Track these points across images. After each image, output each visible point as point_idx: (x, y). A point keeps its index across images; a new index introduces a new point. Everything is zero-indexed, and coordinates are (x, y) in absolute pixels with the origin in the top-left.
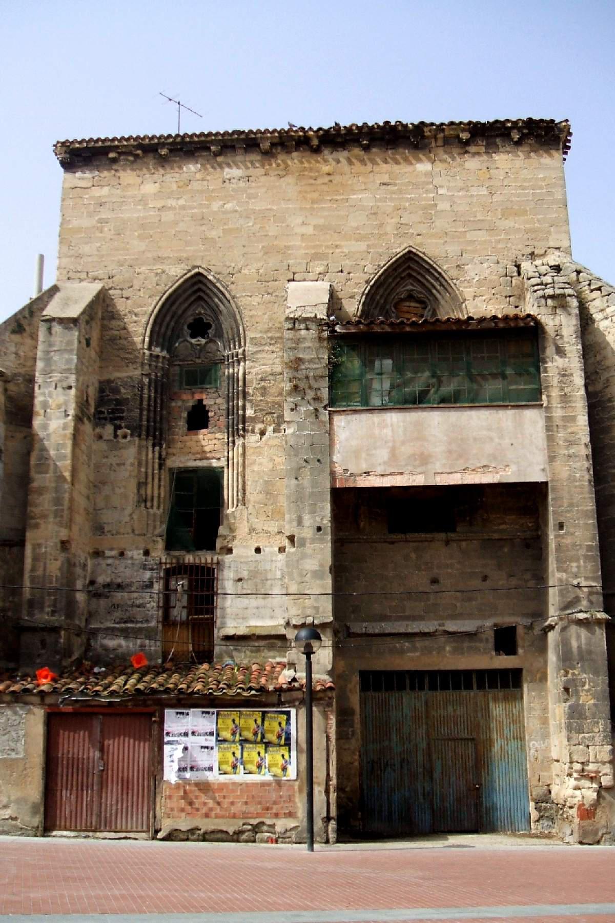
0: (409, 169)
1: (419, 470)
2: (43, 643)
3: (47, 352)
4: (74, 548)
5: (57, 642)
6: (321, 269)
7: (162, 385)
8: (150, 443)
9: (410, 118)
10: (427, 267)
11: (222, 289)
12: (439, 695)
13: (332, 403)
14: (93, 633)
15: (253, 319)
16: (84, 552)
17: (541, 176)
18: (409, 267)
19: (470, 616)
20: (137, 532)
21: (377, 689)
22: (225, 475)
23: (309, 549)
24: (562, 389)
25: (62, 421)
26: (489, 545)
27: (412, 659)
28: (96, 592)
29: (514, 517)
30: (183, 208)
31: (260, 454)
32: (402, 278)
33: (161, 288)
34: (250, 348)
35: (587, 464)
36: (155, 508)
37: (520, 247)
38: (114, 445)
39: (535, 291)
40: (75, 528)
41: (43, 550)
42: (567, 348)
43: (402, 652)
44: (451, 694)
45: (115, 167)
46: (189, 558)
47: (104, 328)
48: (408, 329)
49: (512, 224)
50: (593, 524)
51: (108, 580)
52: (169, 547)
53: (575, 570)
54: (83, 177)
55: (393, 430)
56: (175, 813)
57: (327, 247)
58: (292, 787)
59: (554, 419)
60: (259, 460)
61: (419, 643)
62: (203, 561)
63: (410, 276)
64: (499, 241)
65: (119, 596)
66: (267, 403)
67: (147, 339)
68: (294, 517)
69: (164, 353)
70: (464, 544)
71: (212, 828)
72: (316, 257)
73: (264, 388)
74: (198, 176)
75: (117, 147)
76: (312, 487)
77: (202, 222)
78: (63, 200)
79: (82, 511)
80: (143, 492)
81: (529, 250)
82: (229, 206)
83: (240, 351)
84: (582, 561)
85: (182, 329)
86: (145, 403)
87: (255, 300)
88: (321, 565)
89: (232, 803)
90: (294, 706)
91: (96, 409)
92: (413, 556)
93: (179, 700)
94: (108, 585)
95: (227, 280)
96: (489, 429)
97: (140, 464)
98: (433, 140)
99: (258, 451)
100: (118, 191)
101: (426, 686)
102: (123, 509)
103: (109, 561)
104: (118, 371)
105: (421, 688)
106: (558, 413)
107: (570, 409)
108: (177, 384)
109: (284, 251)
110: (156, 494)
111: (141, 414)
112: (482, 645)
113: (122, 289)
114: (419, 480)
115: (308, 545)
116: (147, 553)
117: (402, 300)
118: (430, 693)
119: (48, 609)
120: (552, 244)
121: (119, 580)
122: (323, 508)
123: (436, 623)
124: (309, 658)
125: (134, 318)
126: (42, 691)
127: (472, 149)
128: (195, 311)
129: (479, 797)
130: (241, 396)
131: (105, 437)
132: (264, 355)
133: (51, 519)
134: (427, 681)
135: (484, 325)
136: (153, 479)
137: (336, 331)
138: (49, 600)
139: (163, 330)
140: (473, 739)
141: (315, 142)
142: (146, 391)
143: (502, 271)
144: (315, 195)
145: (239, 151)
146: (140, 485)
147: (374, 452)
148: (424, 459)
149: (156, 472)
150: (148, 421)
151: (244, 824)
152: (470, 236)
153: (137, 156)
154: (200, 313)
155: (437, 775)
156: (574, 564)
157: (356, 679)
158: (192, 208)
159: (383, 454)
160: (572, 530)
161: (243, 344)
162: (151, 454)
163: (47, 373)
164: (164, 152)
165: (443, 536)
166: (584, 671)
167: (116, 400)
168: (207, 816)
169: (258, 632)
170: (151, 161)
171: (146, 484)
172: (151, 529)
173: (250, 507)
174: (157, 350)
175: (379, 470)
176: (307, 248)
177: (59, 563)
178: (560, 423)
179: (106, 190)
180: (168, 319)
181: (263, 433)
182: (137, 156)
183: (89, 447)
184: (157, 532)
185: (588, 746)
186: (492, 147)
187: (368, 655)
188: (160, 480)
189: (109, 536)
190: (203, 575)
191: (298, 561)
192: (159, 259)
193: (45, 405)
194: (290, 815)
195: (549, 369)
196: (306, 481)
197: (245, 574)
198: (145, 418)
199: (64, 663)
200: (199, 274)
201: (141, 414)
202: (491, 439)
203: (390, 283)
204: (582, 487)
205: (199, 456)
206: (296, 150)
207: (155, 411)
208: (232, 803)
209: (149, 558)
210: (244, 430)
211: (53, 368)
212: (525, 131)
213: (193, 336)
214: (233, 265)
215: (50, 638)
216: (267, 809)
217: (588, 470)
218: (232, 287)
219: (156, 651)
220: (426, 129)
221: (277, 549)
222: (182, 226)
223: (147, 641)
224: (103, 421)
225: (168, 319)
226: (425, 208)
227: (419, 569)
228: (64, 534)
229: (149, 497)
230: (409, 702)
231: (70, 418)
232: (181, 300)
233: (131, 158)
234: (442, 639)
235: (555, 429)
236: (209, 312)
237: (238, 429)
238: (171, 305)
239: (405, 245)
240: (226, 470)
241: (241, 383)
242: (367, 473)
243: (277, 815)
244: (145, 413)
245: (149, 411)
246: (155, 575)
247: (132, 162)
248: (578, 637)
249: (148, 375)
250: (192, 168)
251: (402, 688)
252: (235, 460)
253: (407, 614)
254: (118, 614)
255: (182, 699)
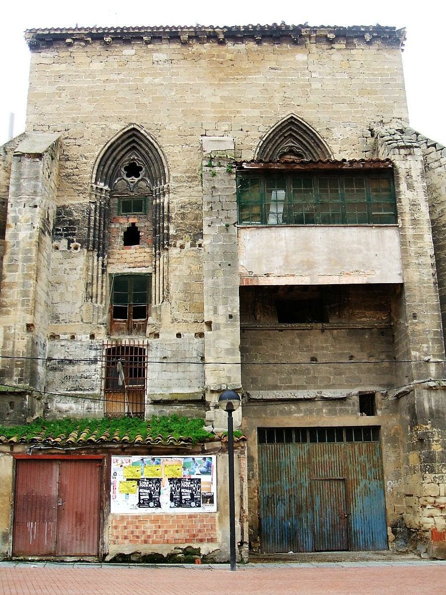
0: (292, 59)
1: (307, 273)
2: (11, 404)
3: (18, 180)
4: (36, 330)
5: (22, 404)
6: (226, 128)
7: (105, 211)
8: (95, 254)
9: (292, 21)
10: (305, 129)
11: (152, 140)
12: (318, 446)
13: (240, 221)
14: (51, 397)
15: (175, 164)
16: (44, 335)
17: (386, 67)
18: (291, 129)
19: (341, 386)
20: (84, 321)
21: (271, 441)
22: (153, 279)
23: (223, 331)
24: (412, 215)
25: (29, 232)
26: (354, 332)
27: (296, 419)
28: (57, 365)
29: (372, 312)
30: (122, 81)
31: (180, 263)
32: (285, 137)
33: (106, 138)
34: (172, 184)
35: (433, 270)
36: (99, 303)
37: (372, 116)
38: (67, 256)
39: (389, 144)
40: (38, 315)
41: (13, 331)
42: (415, 184)
43: (290, 413)
44: (327, 445)
45: (71, 49)
46: (126, 340)
47: (62, 167)
48: (298, 167)
49: (366, 100)
50: (438, 315)
51: (62, 358)
52: (108, 334)
53: (425, 349)
54: (47, 55)
55: (286, 242)
56: (120, 540)
57: (230, 112)
58: (214, 517)
59: (408, 237)
60: (180, 267)
61: (303, 406)
62: (136, 343)
63: (291, 135)
64: (357, 112)
65: (70, 369)
66: (186, 225)
67: (94, 176)
68: (211, 307)
69: (107, 188)
70: (335, 331)
71: (149, 552)
72: (222, 119)
73: (183, 214)
74: (134, 58)
75: (72, 35)
76: (225, 284)
77: (137, 92)
78: (31, 72)
79: (43, 303)
80: (89, 290)
81: (379, 119)
82: (157, 81)
83: (165, 186)
84: (430, 343)
85: (120, 171)
86: (92, 223)
87: (177, 149)
88: (232, 344)
89: (166, 532)
90: (215, 454)
91: (54, 227)
92: (297, 340)
93: (123, 449)
94: (62, 361)
95: (155, 134)
96: (359, 243)
97: (88, 269)
98: (308, 39)
99: (179, 260)
100: (74, 68)
101: (308, 439)
102: (74, 303)
103: (63, 343)
104: (72, 199)
105: (305, 441)
106: (410, 232)
107: (419, 230)
108: (116, 211)
109: (198, 114)
110: (99, 293)
111: (89, 231)
112: (350, 408)
113: (75, 139)
114: (306, 281)
115: (222, 329)
116: (92, 337)
117: (285, 154)
118: (311, 445)
119: (15, 378)
120: (395, 115)
121: (71, 358)
122: (232, 301)
123: (316, 391)
124: (230, 415)
125: (85, 160)
126: (12, 442)
127: (336, 46)
128: (131, 156)
129: (348, 523)
130: (166, 219)
131: (61, 249)
132: (183, 189)
133: (19, 307)
134: (308, 434)
135: (355, 166)
136: (97, 281)
137: (243, 168)
138: (16, 371)
139: (106, 170)
140: (344, 480)
141: (221, 37)
142: (93, 214)
143: (360, 134)
144: (221, 75)
145: (164, 42)
146: (88, 285)
147: (272, 259)
148: (310, 265)
149: (99, 275)
150: (94, 237)
151: (175, 548)
152: (335, 108)
153: (87, 42)
154: (132, 160)
155: (317, 508)
156: (425, 345)
157: (255, 433)
158: (128, 81)
159: (278, 261)
160: (422, 320)
161: (167, 181)
162: (96, 262)
163: (17, 195)
164: (108, 39)
165: (320, 325)
166: (433, 426)
167: (70, 220)
168: (146, 542)
169: (179, 398)
170: (98, 47)
171: (92, 284)
172: (96, 317)
173: (173, 302)
174: (101, 185)
175: (276, 272)
176: (214, 112)
177: (25, 342)
178: (412, 240)
179: (63, 67)
180: (109, 162)
181: (182, 247)
182: (87, 42)
183: (49, 255)
184: (100, 321)
185: (438, 484)
186: (349, 45)
187: (264, 416)
188: (102, 282)
189: (63, 323)
190: (136, 354)
191: (214, 341)
192: (104, 118)
193: (16, 220)
194: (212, 540)
195: (402, 200)
196: (220, 280)
197: (169, 354)
198: (92, 234)
199: (28, 421)
200: (134, 129)
201: (89, 231)
202: (360, 251)
203: (277, 140)
204: (429, 287)
205: (132, 265)
206: (208, 42)
207: (99, 230)
208: (166, 532)
209: (94, 341)
210: (168, 245)
211: (22, 191)
212: (375, 34)
213: (128, 176)
214: (160, 123)
215: (17, 401)
216: (194, 536)
217: (433, 275)
218: (159, 139)
219: (99, 412)
220: (303, 30)
221: (194, 335)
222: (120, 95)
223: (92, 405)
224: (60, 237)
225: (109, 162)
226: (303, 86)
227: (302, 350)
228: (29, 319)
229: (94, 295)
230: (294, 453)
231: (35, 229)
232: (120, 148)
233: (83, 44)
234: (320, 403)
235: (408, 244)
236: (140, 158)
237: (163, 244)
238: (112, 152)
239: (289, 112)
240: (153, 275)
241: (166, 210)
242: (267, 275)
243: (201, 541)
244: (92, 231)
245: (95, 229)
246: (99, 354)
247: (84, 47)
248: (429, 400)
249: (94, 203)
250: (128, 51)
251: (289, 440)
252: (161, 267)
253: (292, 384)
254: (69, 384)
255: (125, 448)
